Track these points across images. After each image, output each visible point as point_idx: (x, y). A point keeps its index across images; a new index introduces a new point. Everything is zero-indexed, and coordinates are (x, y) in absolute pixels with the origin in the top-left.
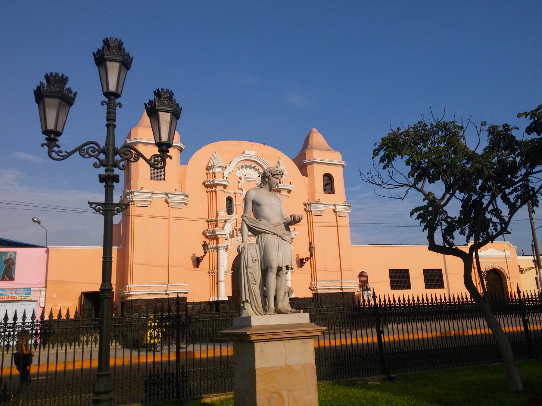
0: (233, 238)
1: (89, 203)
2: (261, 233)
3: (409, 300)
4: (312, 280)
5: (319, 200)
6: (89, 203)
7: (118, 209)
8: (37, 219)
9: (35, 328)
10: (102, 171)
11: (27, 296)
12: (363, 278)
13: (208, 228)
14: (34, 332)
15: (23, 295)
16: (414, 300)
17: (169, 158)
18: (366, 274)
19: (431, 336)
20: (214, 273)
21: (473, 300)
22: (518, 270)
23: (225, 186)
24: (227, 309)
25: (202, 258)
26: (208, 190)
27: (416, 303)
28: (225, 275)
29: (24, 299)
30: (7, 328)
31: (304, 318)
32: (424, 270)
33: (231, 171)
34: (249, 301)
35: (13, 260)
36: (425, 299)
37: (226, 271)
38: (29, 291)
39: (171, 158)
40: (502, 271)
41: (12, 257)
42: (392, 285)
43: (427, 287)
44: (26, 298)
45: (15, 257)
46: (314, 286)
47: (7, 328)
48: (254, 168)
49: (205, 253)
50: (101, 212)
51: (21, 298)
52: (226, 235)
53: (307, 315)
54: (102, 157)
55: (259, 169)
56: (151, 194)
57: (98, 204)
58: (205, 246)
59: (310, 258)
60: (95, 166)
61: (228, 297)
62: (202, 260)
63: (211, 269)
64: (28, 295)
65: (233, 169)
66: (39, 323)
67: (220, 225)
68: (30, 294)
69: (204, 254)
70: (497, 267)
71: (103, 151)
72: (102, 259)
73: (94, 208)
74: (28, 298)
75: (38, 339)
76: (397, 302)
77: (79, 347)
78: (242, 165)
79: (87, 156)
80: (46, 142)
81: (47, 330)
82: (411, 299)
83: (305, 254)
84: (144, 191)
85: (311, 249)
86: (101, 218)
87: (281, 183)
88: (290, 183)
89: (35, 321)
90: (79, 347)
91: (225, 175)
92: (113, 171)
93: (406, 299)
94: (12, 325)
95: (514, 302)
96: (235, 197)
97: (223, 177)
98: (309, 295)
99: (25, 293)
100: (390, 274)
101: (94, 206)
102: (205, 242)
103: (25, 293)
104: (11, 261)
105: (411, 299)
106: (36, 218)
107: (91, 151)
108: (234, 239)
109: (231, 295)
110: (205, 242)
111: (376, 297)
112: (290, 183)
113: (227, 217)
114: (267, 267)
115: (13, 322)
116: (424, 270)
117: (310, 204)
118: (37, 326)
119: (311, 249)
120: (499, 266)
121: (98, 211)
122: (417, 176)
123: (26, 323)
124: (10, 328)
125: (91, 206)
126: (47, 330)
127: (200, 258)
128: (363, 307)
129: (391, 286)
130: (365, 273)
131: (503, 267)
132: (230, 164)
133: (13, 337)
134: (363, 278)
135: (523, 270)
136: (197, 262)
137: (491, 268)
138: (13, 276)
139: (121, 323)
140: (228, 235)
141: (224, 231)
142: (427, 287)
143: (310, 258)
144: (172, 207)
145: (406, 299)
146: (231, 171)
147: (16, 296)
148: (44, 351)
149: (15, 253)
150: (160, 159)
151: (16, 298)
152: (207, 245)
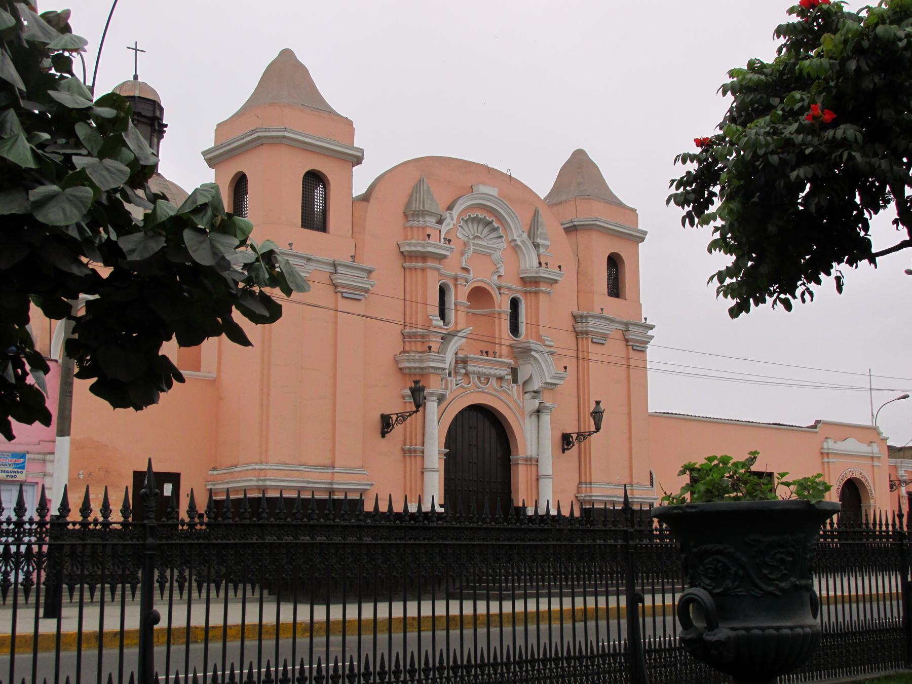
2: (538, 417)
5: (602, 309)
9: (26, 539)
14: (23, 548)
15: (9, 469)
19: (472, 612)
21: (665, 525)
22: (888, 483)
24: (265, 515)
30: (16, 533)
38: (22, 460)
40: (866, 484)
47: (16, 533)
51: (5, 474)
52: (444, 369)
56: (305, 262)
63: (408, 442)
64: (19, 468)
65: (455, 222)
66: (12, 526)
68: (23, 468)
70: (858, 476)
75: (12, 570)
77: (71, 598)
78: (469, 216)
81: (11, 547)
84: (605, 314)
87: (543, 264)
89: (90, 519)
90: (71, 598)
94: (78, 527)
95: (657, 537)
96: (456, 286)
99: (15, 464)
103: (15, 464)
110: (416, 382)
115: (80, 519)
117: (586, 317)
123: (111, 524)
124: (7, 535)
126: (11, 547)
128: (185, 527)
131: (867, 477)
133: (17, 559)
135: (895, 485)
136: (386, 424)
137: (849, 477)
139: (429, 539)
141: (444, 361)
144: (345, 295)
146: (451, 226)
148: (133, 600)
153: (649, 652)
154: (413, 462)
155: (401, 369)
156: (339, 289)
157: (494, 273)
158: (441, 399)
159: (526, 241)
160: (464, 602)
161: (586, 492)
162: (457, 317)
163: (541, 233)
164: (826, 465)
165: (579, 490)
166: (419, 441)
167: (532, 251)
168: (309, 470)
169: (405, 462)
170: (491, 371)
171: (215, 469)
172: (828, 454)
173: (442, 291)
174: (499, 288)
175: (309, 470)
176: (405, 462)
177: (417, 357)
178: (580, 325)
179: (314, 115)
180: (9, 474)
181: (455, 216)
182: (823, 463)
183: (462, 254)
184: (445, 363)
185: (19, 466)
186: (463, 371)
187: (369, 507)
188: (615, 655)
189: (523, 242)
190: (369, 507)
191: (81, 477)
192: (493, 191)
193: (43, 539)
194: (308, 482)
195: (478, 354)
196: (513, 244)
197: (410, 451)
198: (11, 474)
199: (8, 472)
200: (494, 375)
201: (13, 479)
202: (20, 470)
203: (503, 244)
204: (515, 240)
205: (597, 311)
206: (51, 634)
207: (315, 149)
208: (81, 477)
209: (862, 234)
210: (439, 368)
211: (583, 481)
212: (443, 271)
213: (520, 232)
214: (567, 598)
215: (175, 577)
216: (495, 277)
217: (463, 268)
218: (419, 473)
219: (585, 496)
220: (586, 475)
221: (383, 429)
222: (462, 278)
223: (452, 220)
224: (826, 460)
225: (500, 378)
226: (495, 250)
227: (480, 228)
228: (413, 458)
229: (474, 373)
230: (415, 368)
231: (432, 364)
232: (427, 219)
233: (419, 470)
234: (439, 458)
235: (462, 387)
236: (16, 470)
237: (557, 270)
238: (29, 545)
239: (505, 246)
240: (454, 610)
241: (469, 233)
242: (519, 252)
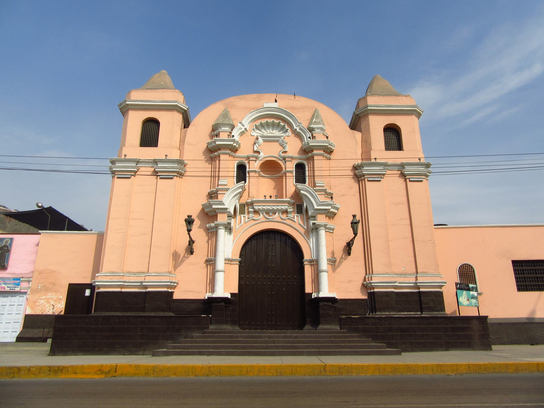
0: (242, 215)
4: (366, 274)
8: (42, 204)
11: (16, 287)
26: (211, 155)
28: (225, 263)
29: (12, 290)
35: (8, 247)
41: (8, 244)
42: (516, 268)
44: (15, 289)
45: (11, 244)
46: (368, 280)
51: (9, 288)
55: (284, 126)
61: (230, 293)
74: (17, 289)
98: (356, 294)
99: (14, 283)
103: (14, 283)
104: (6, 248)
106: (40, 203)
108: (244, 217)
109: (236, 291)
129: (518, 286)
136: (349, 246)
138: (6, 264)
141: (223, 204)
147: (4, 286)
149: (12, 239)
151: (5, 289)
156: (407, 177)
161: (368, 280)
163: (315, 122)
165: (365, 280)
168: (129, 275)
170: (274, 207)
175: (129, 275)
179: (152, 92)
180: (11, 288)
183: (255, 144)
184: (224, 205)
185: (16, 284)
186: (252, 210)
191: (39, 288)
194: (125, 282)
195: (274, 198)
198: (12, 288)
199: (10, 287)
200: (278, 210)
201: (13, 290)
202: (17, 286)
206: (52, 366)
207: (150, 107)
208: (39, 288)
222: (253, 157)
223: (244, 126)
225: (286, 212)
234: (328, 264)
235: (253, 220)
236: (14, 286)
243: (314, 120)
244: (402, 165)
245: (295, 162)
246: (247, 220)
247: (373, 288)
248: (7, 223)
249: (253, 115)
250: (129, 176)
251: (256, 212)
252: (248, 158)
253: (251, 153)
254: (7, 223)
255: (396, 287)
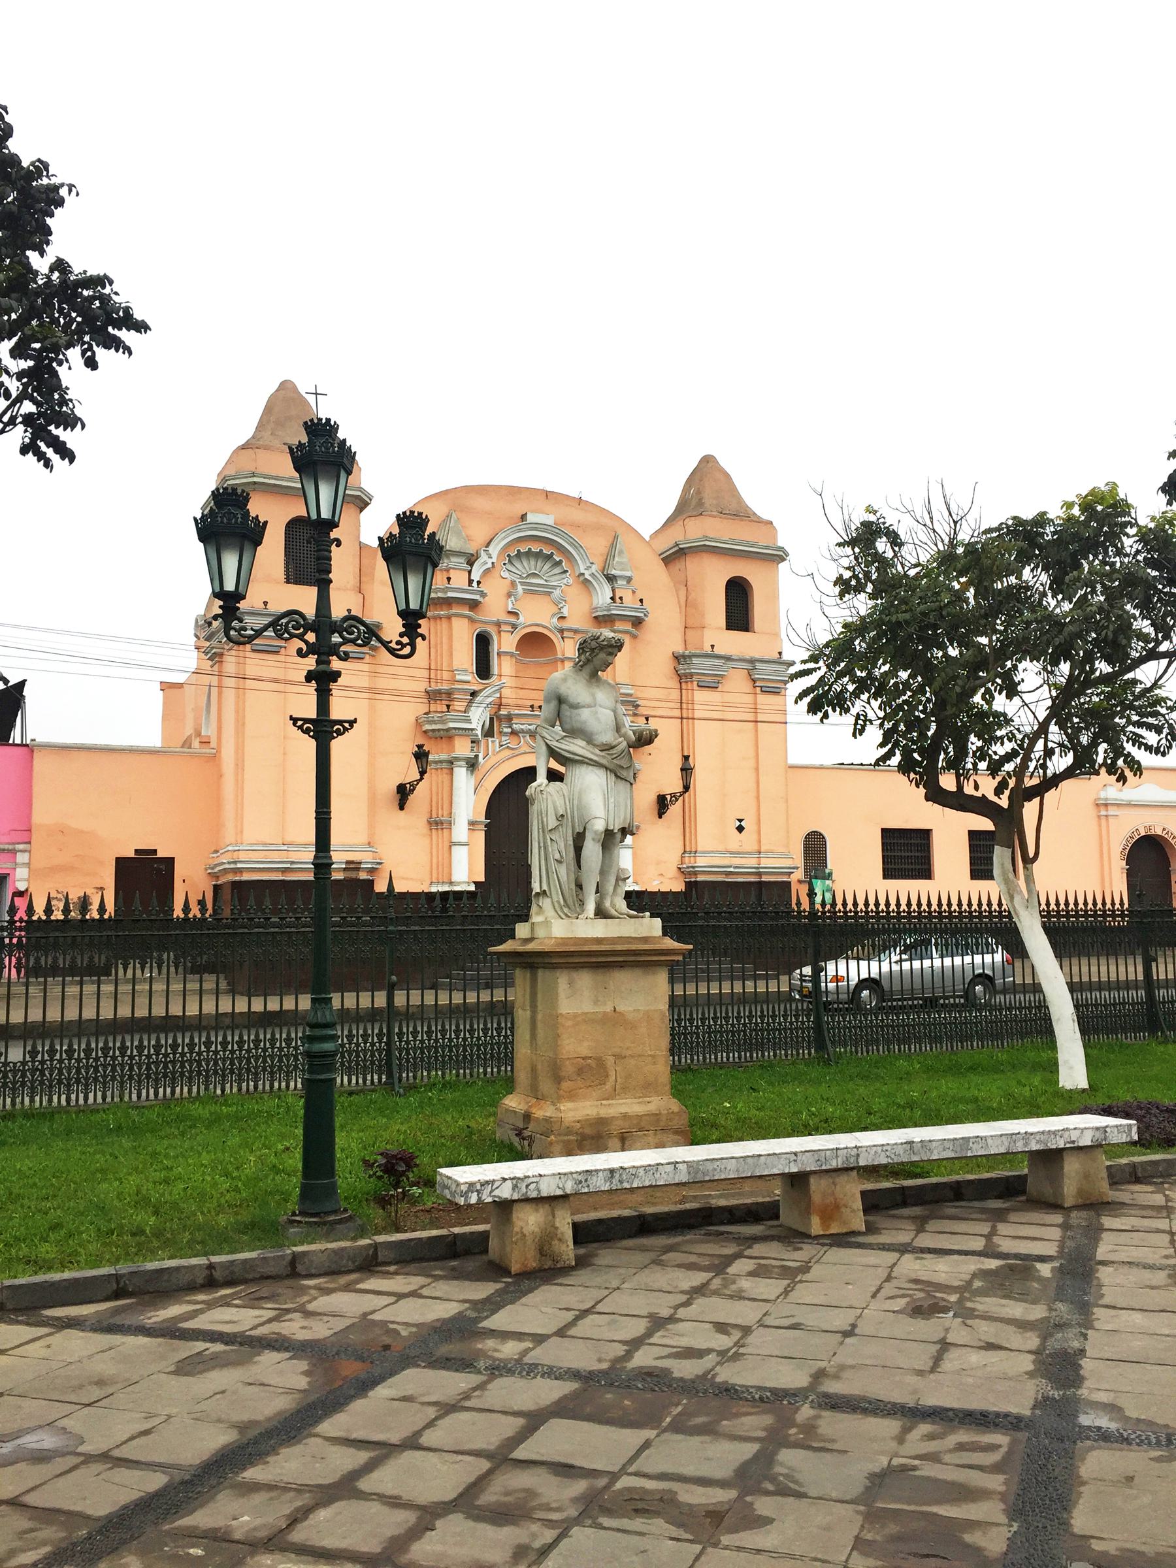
0: (490, 739)
1: (291, 718)
3: (888, 904)
6: (291, 718)
7: (338, 729)
9: (17, 934)
10: (311, 662)
12: (815, 846)
13: (427, 711)
14: (15, 941)
16: (898, 904)
17: (420, 639)
18: (824, 838)
20: (439, 824)
23: (474, 605)
25: (413, 786)
27: (914, 910)
31: (652, 926)
32: (970, 832)
33: (490, 565)
34: (548, 893)
36: (924, 902)
37: (471, 818)
39: (424, 638)
42: (1089, 1050)
43: (888, 874)
48: (538, 555)
49: (422, 773)
50: (312, 734)
52: (472, 730)
53: (658, 922)
54: (311, 637)
57: (306, 721)
58: (421, 756)
59: (682, 794)
60: (300, 653)
62: (412, 791)
65: (494, 560)
67: (459, 705)
69: (681, 789)
70: (1159, 832)
71: (309, 627)
72: (314, 815)
73: (300, 728)
76: (861, 906)
78: (518, 551)
79: (286, 635)
80: (220, 611)
82: (893, 902)
83: (673, 784)
84: (717, 651)
85: (687, 770)
86: (311, 745)
87: (618, 600)
88: (641, 601)
91: (476, 576)
92: (329, 662)
93: (882, 902)
96: (499, 632)
97: (470, 582)
100: (885, 841)
101: (300, 723)
102: (420, 747)
105: (893, 902)
107: (293, 627)
108: (493, 742)
109: (481, 878)
110: (420, 747)
111: (816, 894)
112: (641, 601)
113: (475, 683)
114: (916, 1281)
116: (970, 832)
117: (690, 657)
118: (20, 928)
119: (687, 770)
120: (1164, 829)
121: (307, 732)
122: (975, 597)
125: (294, 724)
127: (408, 786)
130: (821, 834)
131: (1173, 831)
132: (488, 545)
134: (815, 846)
136: (403, 793)
137: (1143, 834)
140: (479, 732)
141: (469, 721)
142: (888, 874)
143: (682, 794)
145: (882, 902)
146: (490, 565)
150: (405, 640)
152: (427, 754)
153: (1164, 1003)
154: (440, 837)
155: (425, 732)
157: (553, 616)
158: (472, 765)
159: (596, 574)
160: (867, 976)
162: (503, 667)
164: (1103, 821)
166: (445, 814)
167: (605, 586)
169: (431, 836)
171: (216, 852)
172: (1106, 805)
173: (483, 643)
174: (561, 631)
176: (431, 836)
177: (436, 719)
178: (681, 667)
181: (495, 554)
182: (1099, 817)
186: (509, 730)
187: (381, 887)
188: (1142, 1003)
189: (593, 575)
190: (381, 887)
192: (549, 520)
193: (13, 934)
194: (292, 863)
196: (582, 578)
197: (437, 823)
203: (569, 579)
204: (583, 574)
205: (708, 649)
209: (7, 151)
210: (466, 729)
211: (688, 850)
212: (476, 617)
213: (589, 564)
214: (16, 1050)
215: (13, 964)
216: (555, 620)
217: (509, 612)
218: (446, 848)
219: (688, 867)
220: (691, 843)
221: (659, 810)
222: (506, 623)
224: (1103, 813)
226: (554, 587)
227: (532, 563)
228: (440, 832)
229: (522, 731)
230: (439, 730)
231: (452, 725)
232: (453, 559)
233: (446, 844)
237: (638, 605)
238: (20, 938)
239: (571, 581)
240: (750, 985)
241: (523, 571)
242: (591, 589)
243: (616, 559)
244: (752, 661)
245: (579, 638)
246: (498, 749)
247: (695, 873)
248: (1000, 703)
249: (508, 536)
250: (361, 656)
251: (514, 733)
252: (498, 624)
253: (504, 617)
254: (1000, 703)
255: (728, 874)
